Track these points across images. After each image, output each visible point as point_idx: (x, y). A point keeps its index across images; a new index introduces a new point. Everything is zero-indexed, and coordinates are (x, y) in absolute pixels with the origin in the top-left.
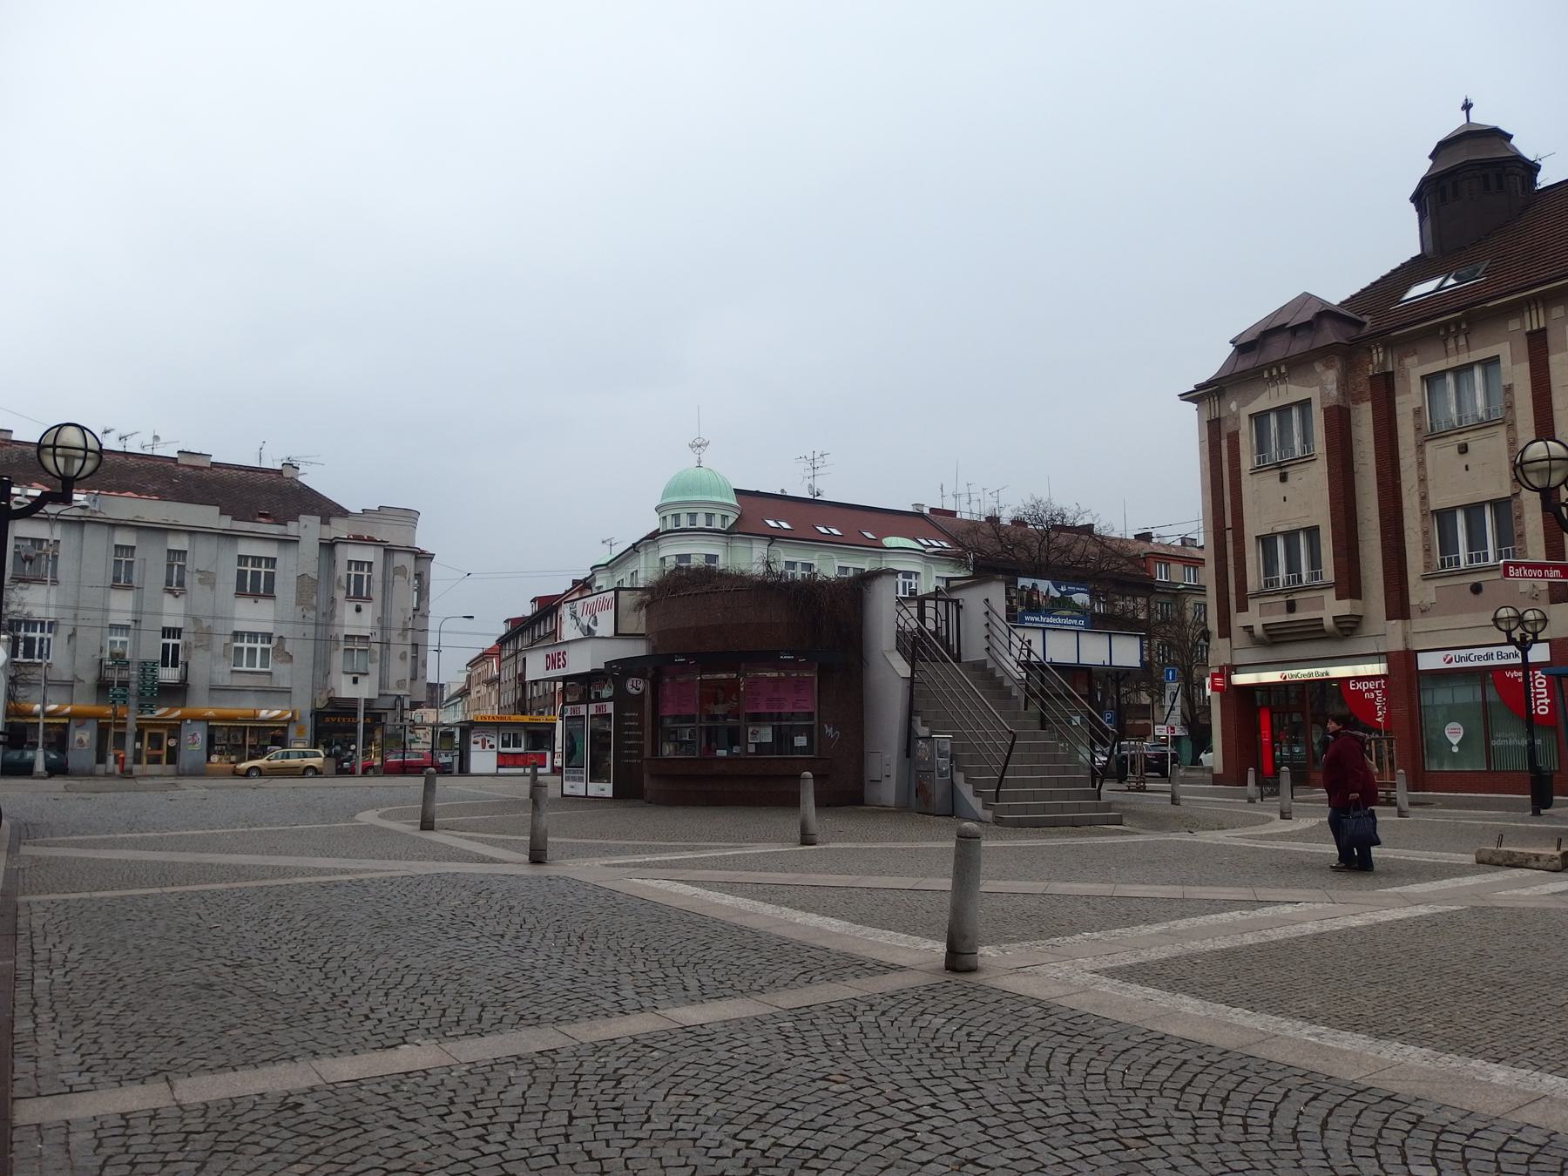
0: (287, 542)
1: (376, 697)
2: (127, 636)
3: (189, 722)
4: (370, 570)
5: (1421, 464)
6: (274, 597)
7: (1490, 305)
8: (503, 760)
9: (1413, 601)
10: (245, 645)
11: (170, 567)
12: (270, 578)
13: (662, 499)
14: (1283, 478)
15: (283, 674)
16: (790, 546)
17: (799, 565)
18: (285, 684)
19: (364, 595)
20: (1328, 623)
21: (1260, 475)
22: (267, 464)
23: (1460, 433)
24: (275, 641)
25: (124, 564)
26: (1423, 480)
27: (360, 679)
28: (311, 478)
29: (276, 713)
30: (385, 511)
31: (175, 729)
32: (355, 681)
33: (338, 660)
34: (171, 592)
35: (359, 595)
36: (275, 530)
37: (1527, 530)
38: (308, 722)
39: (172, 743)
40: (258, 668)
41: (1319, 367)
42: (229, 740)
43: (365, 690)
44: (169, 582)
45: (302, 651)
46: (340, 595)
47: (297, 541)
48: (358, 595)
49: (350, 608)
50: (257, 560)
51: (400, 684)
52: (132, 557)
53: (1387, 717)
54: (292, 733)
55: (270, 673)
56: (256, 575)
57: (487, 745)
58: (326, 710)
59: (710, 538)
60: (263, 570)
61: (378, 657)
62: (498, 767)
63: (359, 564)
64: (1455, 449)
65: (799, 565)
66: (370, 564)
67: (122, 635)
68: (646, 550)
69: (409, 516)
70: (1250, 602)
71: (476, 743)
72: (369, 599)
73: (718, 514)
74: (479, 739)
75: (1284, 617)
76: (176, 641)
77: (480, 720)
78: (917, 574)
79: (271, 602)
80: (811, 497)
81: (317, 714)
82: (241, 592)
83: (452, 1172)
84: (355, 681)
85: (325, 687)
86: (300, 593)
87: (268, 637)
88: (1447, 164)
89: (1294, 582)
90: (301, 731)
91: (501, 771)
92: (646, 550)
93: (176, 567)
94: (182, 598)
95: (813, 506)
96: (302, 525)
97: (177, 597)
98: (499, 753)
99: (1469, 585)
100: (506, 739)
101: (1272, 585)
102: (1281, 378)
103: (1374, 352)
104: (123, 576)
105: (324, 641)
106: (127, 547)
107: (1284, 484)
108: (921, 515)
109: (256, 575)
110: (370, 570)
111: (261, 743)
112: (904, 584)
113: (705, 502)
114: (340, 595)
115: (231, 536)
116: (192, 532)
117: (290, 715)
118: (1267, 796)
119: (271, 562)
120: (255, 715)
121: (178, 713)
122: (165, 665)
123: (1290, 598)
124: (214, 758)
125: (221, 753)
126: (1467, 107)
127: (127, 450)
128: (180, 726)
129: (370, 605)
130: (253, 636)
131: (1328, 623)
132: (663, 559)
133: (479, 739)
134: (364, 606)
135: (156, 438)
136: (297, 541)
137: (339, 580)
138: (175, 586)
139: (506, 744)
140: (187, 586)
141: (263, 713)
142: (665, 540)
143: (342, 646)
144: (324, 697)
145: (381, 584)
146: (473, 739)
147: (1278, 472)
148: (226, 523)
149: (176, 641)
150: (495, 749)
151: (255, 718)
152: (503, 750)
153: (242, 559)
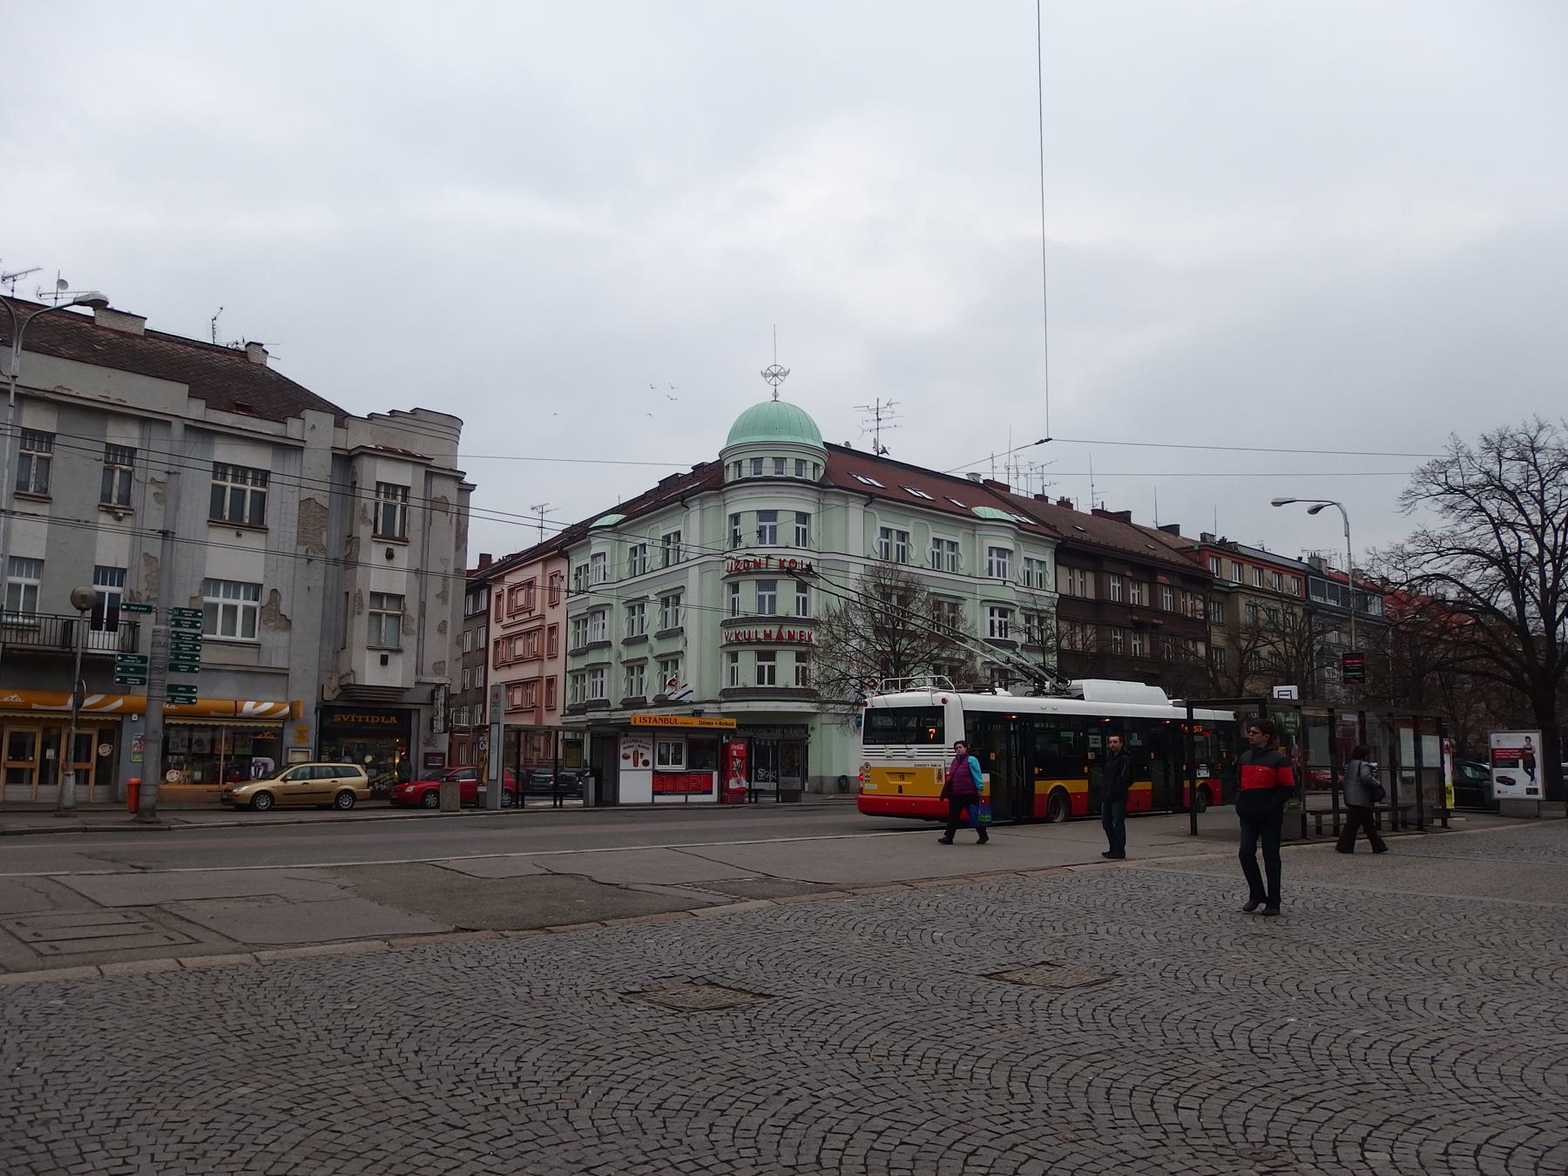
0: (287, 448)
1: (412, 685)
2: (37, 577)
3: (135, 717)
4: (405, 497)
6: (265, 530)
8: (662, 783)
10: (221, 600)
11: (109, 472)
12: (260, 501)
13: (728, 442)
15: (276, 646)
16: (886, 508)
17: (894, 533)
18: (279, 662)
19: (397, 535)
22: (223, 340)
24: (265, 595)
25: (34, 461)
27: (392, 658)
28: (286, 363)
29: (267, 706)
30: (421, 416)
31: (111, 730)
32: (384, 661)
33: (360, 629)
34: (110, 511)
35: (390, 536)
36: (268, 428)
38: (311, 720)
39: (105, 750)
40: (238, 637)
42: (190, 747)
43: (396, 675)
44: (106, 496)
45: (305, 610)
46: (365, 532)
47: (302, 449)
48: (388, 535)
49: (376, 554)
50: (240, 472)
51: (439, 668)
52: (49, 451)
54: (289, 738)
55: (258, 645)
56: (238, 495)
57: (640, 761)
58: (339, 704)
59: (800, 491)
60: (249, 487)
61: (415, 628)
62: (655, 793)
63: (391, 489)
65: (894, 533)
66: (406, 489)
67: (28, 576)
68: (701, 504)
69: (450, 425)
71: (626, 757)
72: (404, 541)
73: (811, 460)
74: (630, 752)
76: (115, 589)
77: (638, 723)
78: (1010, 552)
79: (262, 537)
80: (875, 454)
81: (325, 710)
82: (216, 519)
83: (112, 1173)
84: (384, 661)
85: (336, 670)
86: (302, 523)
87: (255, 589)
90: (301, 735)
91: (659, 799)
92: (701, 504)
93: (117, 473)
94: (127, 522)
95: (876, 462)
96: (308, 426)
97: (119, 519)
98: (656, 773)
100: (663, 751)
104: (32, 480)
105: (341, 604)
106: (42, 434)
108: (976, 484)
109: (238, 495)
110: (405, 497)
111: (239, 751)
112: (998, 563)
113: (775, 443)
114: (365, 532)
115: (201, 432)
116: (146, 421)
117: (287, 709)
119: (263, 476)
120: (237, 710)
121: (119, 703)
122: (96, 625)
124: (173, 776)
125: (179, 767)
127: (17, 296)
128: (119, 724)
129: (406, 549)
130: (233, 586)
132: (735, 518)
133: (630, 752)
134: (397, 551)
135: (62, 283)
136: (302, 449)
137: (364, 510)
138: (117, 505)
139: (663, 761)
140: (134, 504)
141: (248, 706)
142: (735, 493)
143: (367, 610)
144: (334, 683)
145: (421, 520)
146: (622, 752)
148: (197, 410)
149: (115, 589)
150: (650, 766)
151: (235, 714)
152: (659, 767)
153: (220, 469)
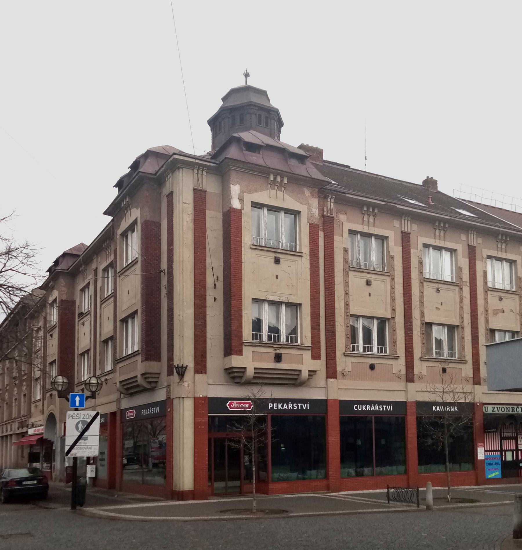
5: (346, 284)
7: (398, 206)
9: (339, 368)
14: (277, 261)
20: (250, 373)
21: (259, 252)
23: (368, 273)
26: (347, 294)
37: (397, 340)
41: (307, 192)
53: (165, 434)
64: (364, 282)
70: (244, 349)
75: (272, 365)
88: (230, 103)
89: (275, 340)
99: (369, 364)
101: (292, 341)
102: (281, 186)
103: (329, 200)
107: (277, 266)
118: (392, 500)
123: (278, 351)
126: (247, 75)
131: (250, 373)
147: (273, 255)
